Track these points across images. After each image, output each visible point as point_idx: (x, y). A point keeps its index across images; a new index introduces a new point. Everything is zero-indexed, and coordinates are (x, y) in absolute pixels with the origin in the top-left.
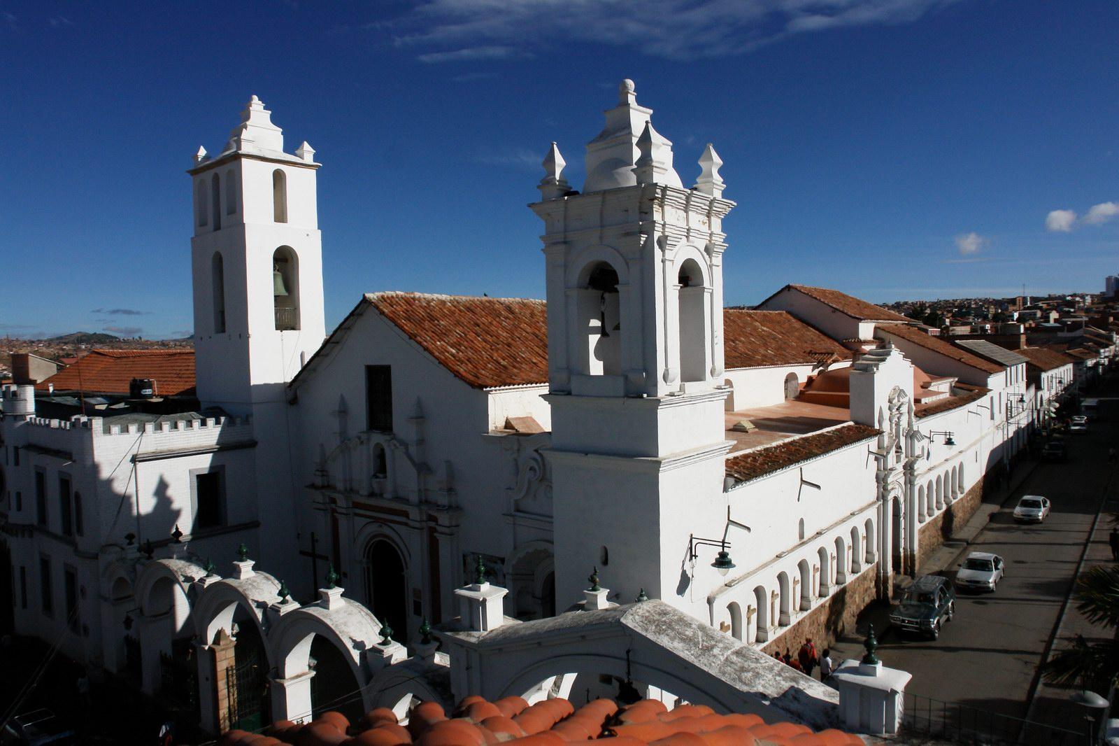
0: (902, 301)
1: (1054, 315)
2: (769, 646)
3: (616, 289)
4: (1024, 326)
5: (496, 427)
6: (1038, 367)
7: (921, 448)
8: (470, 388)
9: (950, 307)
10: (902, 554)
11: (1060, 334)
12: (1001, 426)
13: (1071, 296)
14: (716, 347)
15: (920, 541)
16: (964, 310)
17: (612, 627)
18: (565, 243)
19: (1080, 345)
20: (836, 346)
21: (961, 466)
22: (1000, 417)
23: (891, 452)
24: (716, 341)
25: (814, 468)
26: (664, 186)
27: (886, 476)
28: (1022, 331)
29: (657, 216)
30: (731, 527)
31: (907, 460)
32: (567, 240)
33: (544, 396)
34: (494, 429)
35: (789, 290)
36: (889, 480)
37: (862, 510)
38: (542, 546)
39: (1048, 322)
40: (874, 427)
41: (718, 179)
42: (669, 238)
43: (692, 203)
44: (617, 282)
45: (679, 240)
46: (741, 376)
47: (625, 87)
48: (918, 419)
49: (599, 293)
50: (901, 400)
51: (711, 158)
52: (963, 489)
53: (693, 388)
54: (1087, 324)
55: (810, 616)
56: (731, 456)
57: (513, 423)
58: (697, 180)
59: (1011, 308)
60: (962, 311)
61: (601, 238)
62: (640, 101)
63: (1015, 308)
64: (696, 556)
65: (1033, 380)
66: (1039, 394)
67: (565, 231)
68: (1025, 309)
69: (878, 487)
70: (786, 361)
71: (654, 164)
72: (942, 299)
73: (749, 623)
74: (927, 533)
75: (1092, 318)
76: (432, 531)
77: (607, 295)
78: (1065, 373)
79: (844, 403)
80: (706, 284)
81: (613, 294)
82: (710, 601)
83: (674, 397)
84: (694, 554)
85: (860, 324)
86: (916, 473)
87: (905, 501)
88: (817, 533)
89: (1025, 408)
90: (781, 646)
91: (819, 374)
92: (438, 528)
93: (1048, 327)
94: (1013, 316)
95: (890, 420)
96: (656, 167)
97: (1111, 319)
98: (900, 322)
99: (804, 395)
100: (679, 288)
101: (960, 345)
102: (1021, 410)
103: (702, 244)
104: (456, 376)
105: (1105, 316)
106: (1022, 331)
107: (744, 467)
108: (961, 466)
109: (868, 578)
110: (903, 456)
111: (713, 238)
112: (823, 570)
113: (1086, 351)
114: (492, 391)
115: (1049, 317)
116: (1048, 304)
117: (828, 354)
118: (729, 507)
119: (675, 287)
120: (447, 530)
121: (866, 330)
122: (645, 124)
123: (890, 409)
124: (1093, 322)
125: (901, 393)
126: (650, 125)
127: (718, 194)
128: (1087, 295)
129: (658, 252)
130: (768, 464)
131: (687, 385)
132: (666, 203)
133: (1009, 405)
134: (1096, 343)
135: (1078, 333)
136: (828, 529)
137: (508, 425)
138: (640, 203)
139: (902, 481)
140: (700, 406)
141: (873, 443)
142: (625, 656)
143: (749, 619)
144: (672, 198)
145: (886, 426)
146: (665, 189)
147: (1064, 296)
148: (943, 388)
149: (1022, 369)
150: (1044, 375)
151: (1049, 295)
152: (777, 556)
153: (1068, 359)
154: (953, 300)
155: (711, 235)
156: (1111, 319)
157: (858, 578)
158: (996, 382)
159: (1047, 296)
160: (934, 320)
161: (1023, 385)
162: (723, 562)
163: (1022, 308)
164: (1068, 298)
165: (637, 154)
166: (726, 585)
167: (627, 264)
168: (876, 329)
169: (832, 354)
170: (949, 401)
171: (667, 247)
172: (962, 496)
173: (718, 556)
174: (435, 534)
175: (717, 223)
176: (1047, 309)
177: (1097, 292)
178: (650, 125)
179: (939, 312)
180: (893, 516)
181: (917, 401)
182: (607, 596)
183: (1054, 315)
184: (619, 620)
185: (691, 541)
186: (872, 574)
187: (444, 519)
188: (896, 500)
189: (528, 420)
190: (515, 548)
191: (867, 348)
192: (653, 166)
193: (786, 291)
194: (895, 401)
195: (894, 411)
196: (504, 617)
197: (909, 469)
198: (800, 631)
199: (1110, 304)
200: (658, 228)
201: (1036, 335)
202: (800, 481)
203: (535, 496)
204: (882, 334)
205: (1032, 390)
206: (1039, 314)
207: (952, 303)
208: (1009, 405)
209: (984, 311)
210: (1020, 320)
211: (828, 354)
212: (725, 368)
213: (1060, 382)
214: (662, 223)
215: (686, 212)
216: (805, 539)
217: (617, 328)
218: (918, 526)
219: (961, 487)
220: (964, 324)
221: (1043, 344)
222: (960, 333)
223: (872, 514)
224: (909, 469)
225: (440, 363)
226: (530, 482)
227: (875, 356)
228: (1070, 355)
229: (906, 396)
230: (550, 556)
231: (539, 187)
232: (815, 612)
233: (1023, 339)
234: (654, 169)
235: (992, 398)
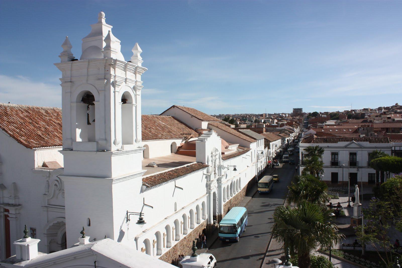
0: (221, 114)
1: (276, 121)
2: (163, 256)
3: (94, 103)
4: (265, 125)
5: (39, 166)
6: (269, 140)
7: (224, 172)
8: (26, 148)
9: (239, 117)
10: (217, 215)
11: (277, 128)
12: (255, 163)
13: (282, 114)
14: (138, 130)
15: (224, 209)
16: (244, 118)
17: (90, 252)
18: (71, 82)
19: (284, 132)
20: (194, 132)
21: (240, 179)
22: (255, 160)
23: (212, 174)
24: (138, 127)
25: (180, 181)
26: (115, 59)
27: (210, 184)
28: (264, 127)
29: (112, 72)
30: (145, 207)
31: (219, 177)
32: (72, 81)
33: (60, 151)
34: (37, 167)
35: (174, 108)
36: (212, 185)
37: (200, 198)
38: (60, 220)
39: (274, 123)
40: (205, 164)
41: (140, 58)
42: (117, 82)
43: (128, 67)
44: (94, 100)
45: (122, 83)
46: (151, 144)
47: (101, 14)
48: (223, 160)
49: (87, 105)
50: (216, 153)
51: (137, 49)
52: (240, 187)
53: (127, 147)
54: (286, 124)
55: (180, 243)
56: (145, 177)
57: (47, 164)
58: (131, 58)
59: (261, 118)
60: (244, 118)
61: (87, 80)
62: (107, 22)
63: (262, 118)
64: (129, 220)
65: (267, 145)
66: (269, 150)
67: (71, 77)
68: (266, 118)
69: (207, 189)
70: (172, 138)
71: (111, 49)
72: (236, 113)
73: (154, 247)
74: (227, 206)
75: (288, 122)
76: (6, 216)
77: (90, 106)
78: (278, 143)
79: (194, 155)
80: (134, 102)
81: (93, 106)
82: (136, 239)
83: (118, 151)
84: (128, 219)
85: (202, 122)
86: (222, 182)
87: (218, 194)
88: (182, 208)
89: (264, 156)
90: (168, 256)
91: (185, 143)
92: (9, 215)
93: (273, 125)
94: (262, 121)
95: (212, 161)
96: (112, 51)
97: (294, 123)
98: (218, 122)
99: (178, 151)
100: (122, 104)
101: (240, 131)
102: (262, 157)
103: (132, 85)
104: (18, 142)
105: (292, 121)
106: (264, 127)
107: (150, 181)
108: (240, 179)
109: (204, 225)
110: (217, 175)
111: (137, 83)
112: (184, 223)
113: (286, 135)
114: (36, 149)
115: (274, 122)
116: (274, 117)
117: (189, 134)
118: (144, 198)
119: (120, 104)
120: (14, 216)
121: (204, 125)
122: (108, 32)
123: (212, 157)
124: (288, 124)
125: (217, 150)
126: (111, 33)
127: (140, 65)
128: (287, 114)
129: (112, 89)
130: (160, 180)
131: (125, 146)
132: (116, 67)
133: (258, 155)
134: (289, 131)
135: (283, 128)
136: (187, 206)
137: (44, 165)
138: (105, 66)
139: (217, 185)
140: (131, 155)
141: (205, 171)
142: (94, 264)
143: (154, 245)
144: (119, 65)
145: (210, 163)
146: (116, 61)
147: (279, 114)
148: (234, 148)
149: (263, 141)
150: (271, 144)
151: (274, 113)
152: (165, 219)
153: (279, 137)
154: (241, 114)
155: (136, 82)
156: (294, 123)
157: (199, 226)
158: (253, 146)
159: (274, 114)
160: (232, 122)
161: (263, 146)
162: (141, 222)
163: (265, 118)
164: (281, 115)
165: (104, 44)
166: (143, 232)
167: (99, 93)
168: (208, 124)
169: (190, 134)
170: (235, 153)
171: (116, 86)
172: (240, 191)
173: (139, 219)
174: (8, 218)
175: (139, 77)
176: (273, 119)
177: (290, 113)
178: (111, 33)
179: (235, 119)
180: (213, 200)
181: (223, 153)
182: (89, 240)
183: (276, 121)
184: (91, 248)
185: (127, 214)
186: (205, 224)
187: (12, 210)
188: (214, 194)
189: (55, 163)
190: (48, 222)
191: (204, 132)
192: (111, 50)
193: (173, 108)
194: (214, 154)
195: (213, 157)
196: (38, 253)
197: (219, 181)
198: (176, 249)
199: (294, 117)
200: (112, 77)
201: (269, 128)
202: (175, 187)
203: (57, 197)
204: (211, 127)
205: (267, 148)
206: (271, 120)
207: (240, 115)
208: (258, 155)
209: (252, 119)
210: (264, 122)
211: (189, 134)
212: (142, 140)
213: (276, 146)
214: (114, 75)
215: (125, 71)
216: (177, 211)
217: (94, 121)
218: (223, 203)
219: (240, 187)
220: (244, 124)
221: (270, 131)
222: (242, 127)
223: (205, 199)
224: (219, 181)
225: (10, 136)
226: (55, 191)
227: (205, 135)
228: (280, 136)
229: (218, 151)
230: (64, 224)
231: (59, 56)
232: (182, 241)
233: (264, 129)
234: (112, 52)
235: (252, 152)
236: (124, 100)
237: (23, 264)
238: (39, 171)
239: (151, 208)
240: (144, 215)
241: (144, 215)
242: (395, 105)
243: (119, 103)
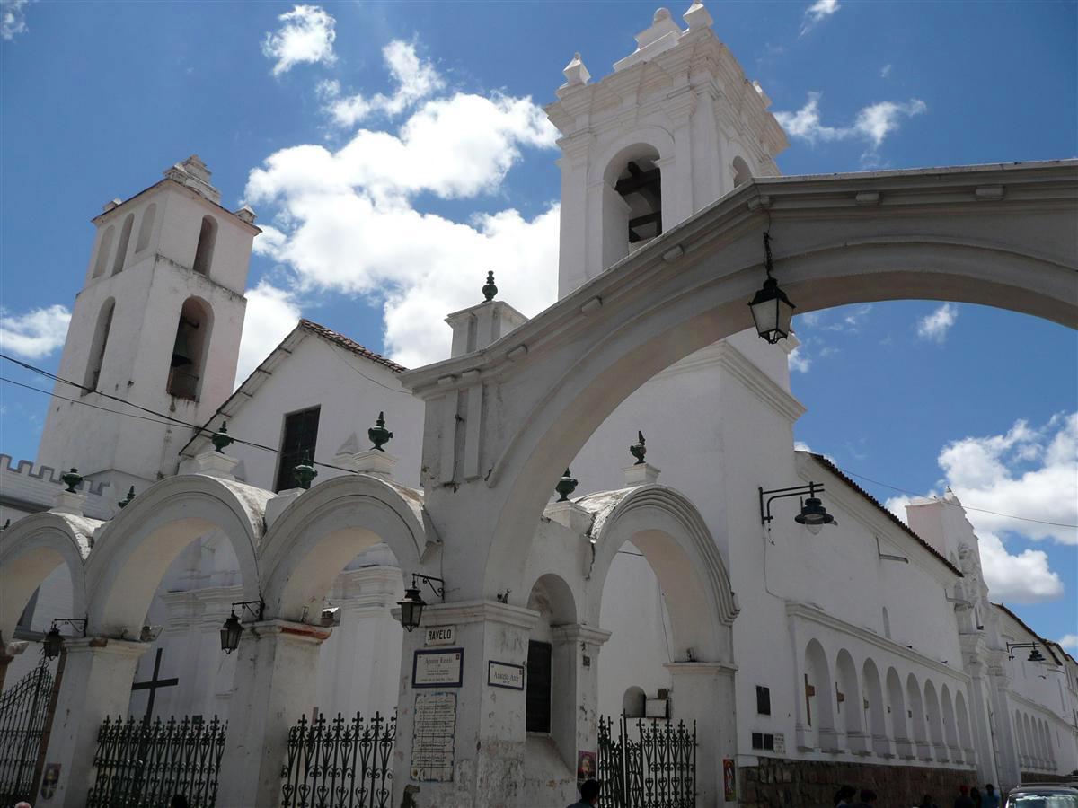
64: (769, 518)
84: (766, 515)
236: (841, 698)
237: (598, 526)
238: (415, 517)
239: (904, 563)
240: (823, 490)
241: (823, 490)
242: (762, 288)
243: (822, 487)
